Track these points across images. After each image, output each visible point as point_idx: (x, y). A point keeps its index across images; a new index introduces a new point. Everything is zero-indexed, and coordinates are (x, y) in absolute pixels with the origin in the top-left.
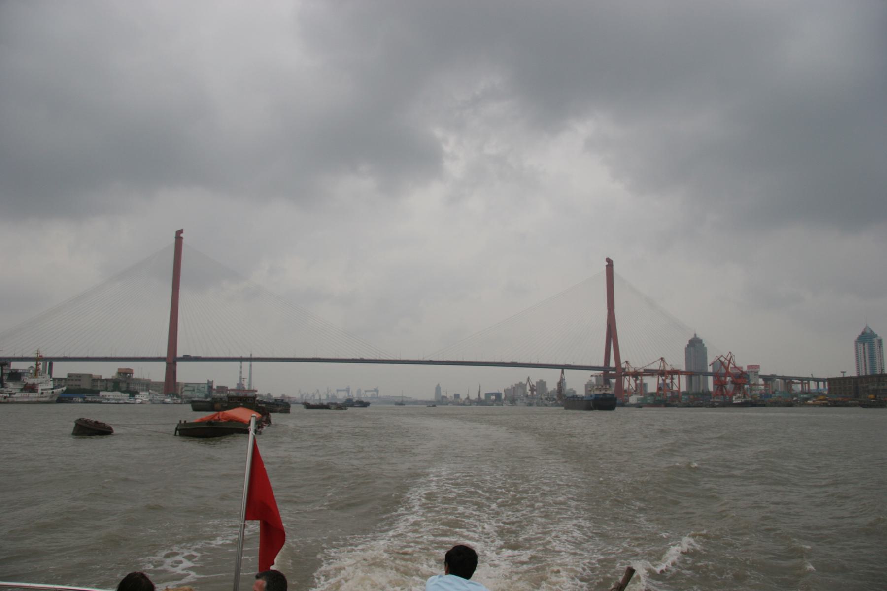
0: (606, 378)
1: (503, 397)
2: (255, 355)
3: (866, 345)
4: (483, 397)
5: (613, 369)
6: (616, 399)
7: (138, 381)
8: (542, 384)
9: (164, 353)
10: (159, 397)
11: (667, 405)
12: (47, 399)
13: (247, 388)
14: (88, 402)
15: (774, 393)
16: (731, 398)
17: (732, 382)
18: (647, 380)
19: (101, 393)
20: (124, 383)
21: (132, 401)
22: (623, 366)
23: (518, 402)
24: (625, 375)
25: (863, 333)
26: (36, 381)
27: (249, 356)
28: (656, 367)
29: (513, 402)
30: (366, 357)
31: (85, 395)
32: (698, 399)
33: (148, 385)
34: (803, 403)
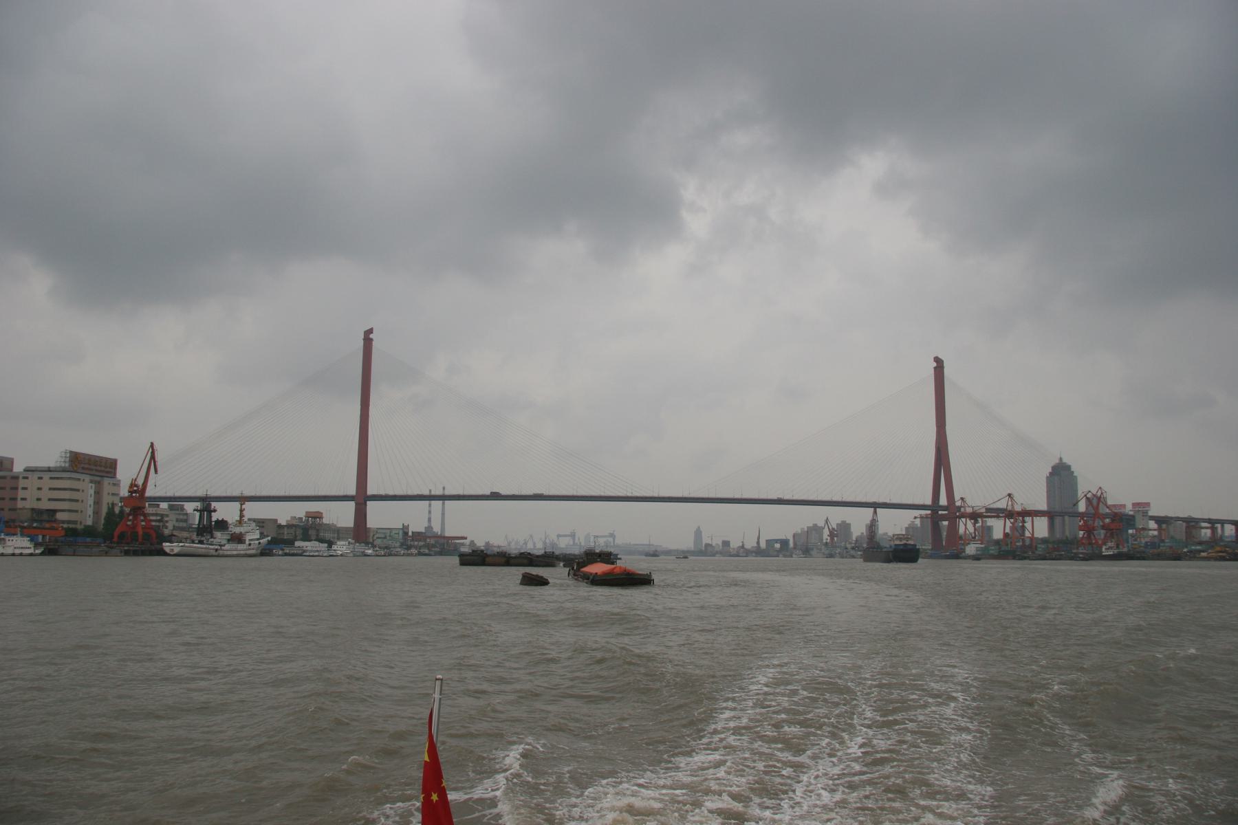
1: (791, 544)
2: (450, 491)
4: (763, 545)
5: (944, 508)
8: (845, 527)
9: (352, 491)
10: (360, 548)
12: (253, 552)
14: (286, 554)
18: (990, 522)
19: (297, 544)
22: (958, 504)
23: (814, 553)
24: (960, 517)
28: (1002, 505)
29: (807, 551)
30: (546, 493)
32: (1057, 550)
33: (340, 533)
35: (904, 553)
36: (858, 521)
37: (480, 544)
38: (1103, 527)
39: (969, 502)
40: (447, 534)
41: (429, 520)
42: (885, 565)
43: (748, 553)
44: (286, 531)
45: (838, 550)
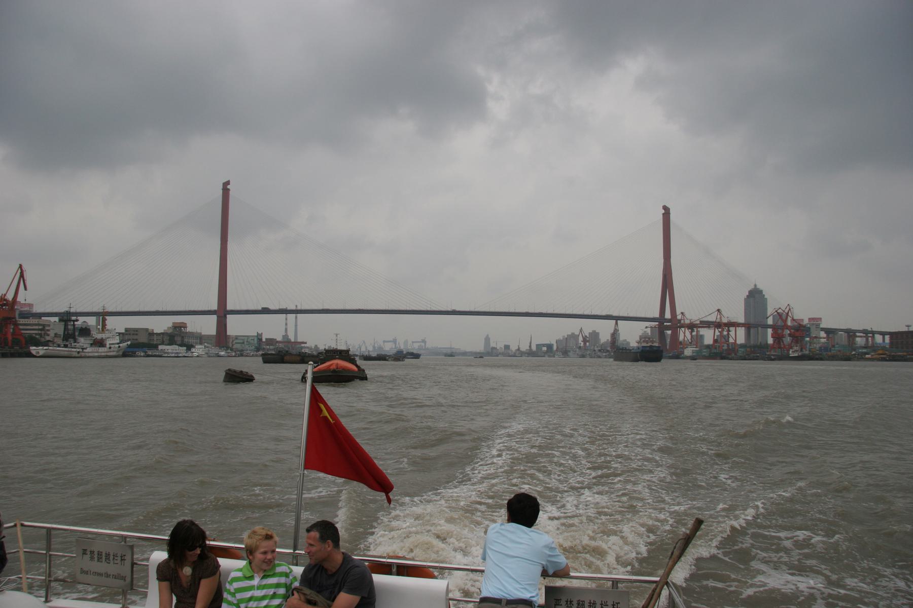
0: (661, 329)
1: (555, 348)
4: (534, 348)
6: (662, 351)
7: (192, 335)
8: (595, 335)
10: (215, 350)
11: (723, 358)
12: (114, 354)
13: (293, 340)
14: (149, 356)
15: (833, 346)
16: (788, 351)
17: (790, 335)
19: (160, 347)
21: (189, 354)
22: (679, 317)
23: (571, 354)
24: (681, 327)
26: (103, 336)
27: (293, 308)
28: (712, 318)
29: (565, 353)
31: (146, 349)
32: (754, 352)
33: (201, 339)
34: (861, 357)
37: (322, 348)
39: (688, 316)
41: (286, 330)
44: (155, 337)
45: (588, 352)
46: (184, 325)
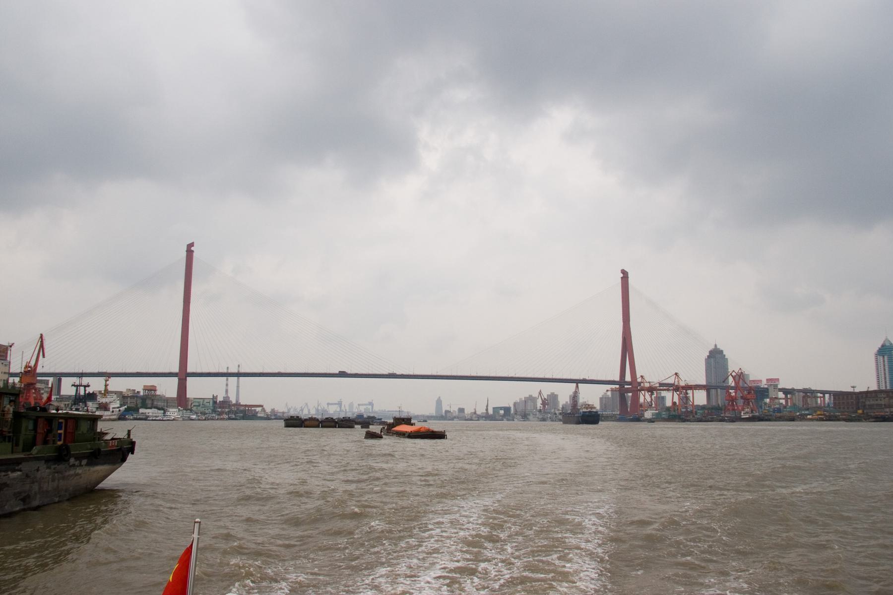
1: (512, 412)
3: (886, 358)
4: (491, 412)
8: (554, 397)
9: (176, 369)
10: (187, 414)
11: (684, 421)
13: (234, 402)
18: (664, 393)
19: (141, 411)
20: (149, 399)
22: (639, 380)
23: (531, 417)
24: (640, 390)
25: (883, 346)
27: (235, 371)
29: (525, 416)
32: (709, 414)
35: (590, 418)
36: (564, 394)
38: (742, 398)
40: (243, 402)
41: (227, 391)
42: (574, 426)
43: (479, 417)
46: (153, 389)
